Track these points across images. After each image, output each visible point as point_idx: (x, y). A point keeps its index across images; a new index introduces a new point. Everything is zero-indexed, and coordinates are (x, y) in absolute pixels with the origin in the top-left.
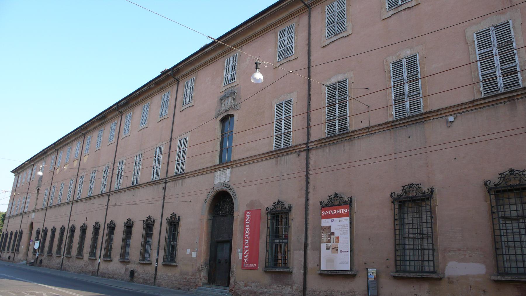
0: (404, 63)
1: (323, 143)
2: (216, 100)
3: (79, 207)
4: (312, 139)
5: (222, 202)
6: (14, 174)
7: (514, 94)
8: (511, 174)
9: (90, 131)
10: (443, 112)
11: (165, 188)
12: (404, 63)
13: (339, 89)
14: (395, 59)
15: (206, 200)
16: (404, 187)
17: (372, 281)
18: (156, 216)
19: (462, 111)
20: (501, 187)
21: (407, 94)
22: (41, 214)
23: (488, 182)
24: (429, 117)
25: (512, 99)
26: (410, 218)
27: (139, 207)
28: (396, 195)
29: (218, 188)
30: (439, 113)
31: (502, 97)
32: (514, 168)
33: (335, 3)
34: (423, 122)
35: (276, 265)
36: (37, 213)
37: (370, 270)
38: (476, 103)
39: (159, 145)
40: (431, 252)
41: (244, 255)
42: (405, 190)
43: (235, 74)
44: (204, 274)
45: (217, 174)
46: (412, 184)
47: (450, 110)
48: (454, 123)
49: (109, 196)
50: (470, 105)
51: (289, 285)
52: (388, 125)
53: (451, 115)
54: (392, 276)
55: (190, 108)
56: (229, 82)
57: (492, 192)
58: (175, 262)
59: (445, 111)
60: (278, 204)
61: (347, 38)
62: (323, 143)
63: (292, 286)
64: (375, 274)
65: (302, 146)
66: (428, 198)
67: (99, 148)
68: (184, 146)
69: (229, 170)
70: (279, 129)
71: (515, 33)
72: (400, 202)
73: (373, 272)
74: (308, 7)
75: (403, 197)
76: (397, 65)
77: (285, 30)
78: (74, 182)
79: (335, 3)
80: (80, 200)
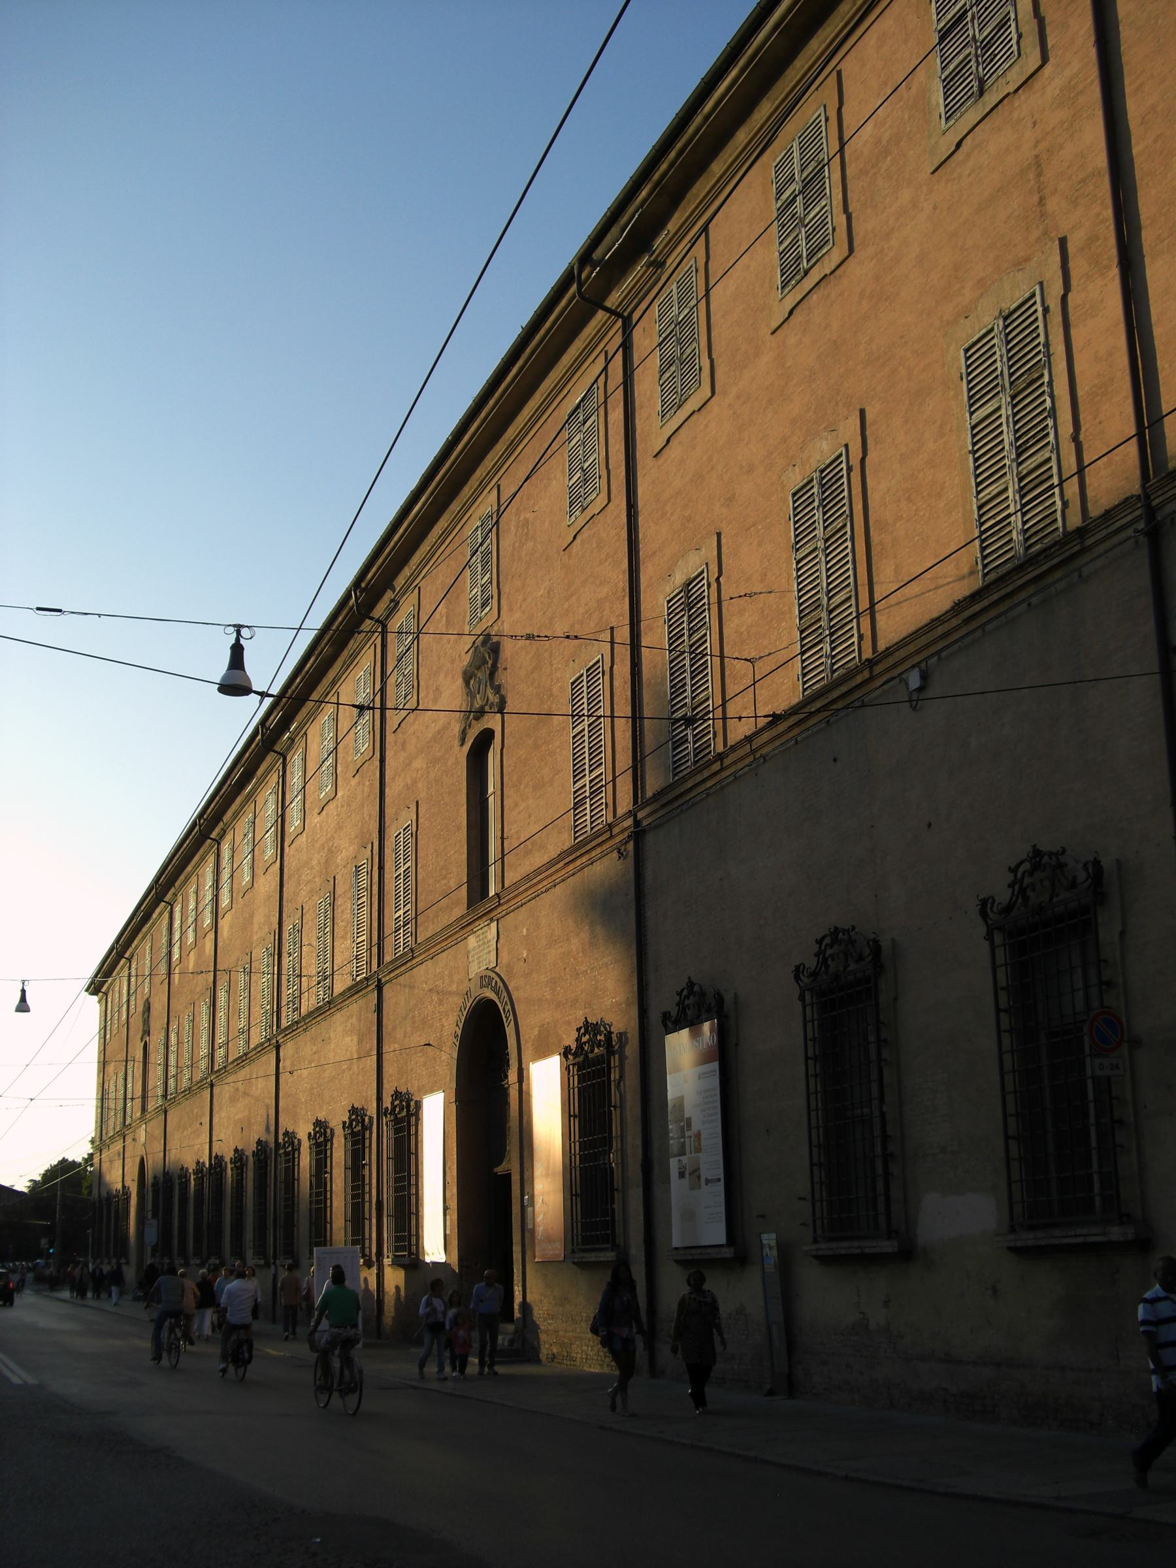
6: (95, 998)
19: (940, 645)
27: (326, 1081)
60: (1036, 867)
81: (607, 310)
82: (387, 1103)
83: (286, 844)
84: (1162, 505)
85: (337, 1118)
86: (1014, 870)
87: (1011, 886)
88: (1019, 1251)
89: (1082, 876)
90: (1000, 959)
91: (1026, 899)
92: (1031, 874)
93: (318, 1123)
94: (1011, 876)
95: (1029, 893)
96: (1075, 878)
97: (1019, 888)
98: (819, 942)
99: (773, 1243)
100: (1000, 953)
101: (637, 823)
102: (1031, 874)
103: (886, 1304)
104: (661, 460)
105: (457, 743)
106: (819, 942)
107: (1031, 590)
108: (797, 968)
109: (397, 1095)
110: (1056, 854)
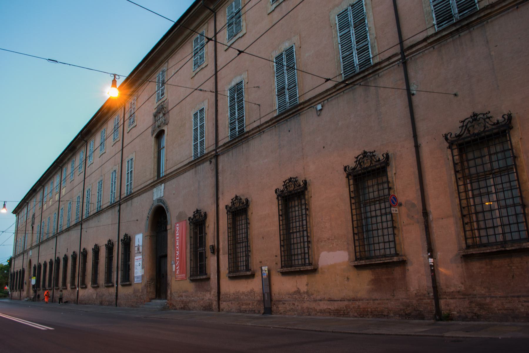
0: (284, 56)
1: (433, 42)
2: (152, 117)
3: (62, 238)
4: (220, 144)
5: (159, 216)
6: (15, 215)
7: (366, 73)
8: (473, 120)
9: (65, 163)
10: (313, 101)
11: (119, 211)
12: (284, 56)
13: (237, 91)
14: (277, 53)
15: (148, 217)
16: (357, 158)
17: (265, 279)
18: (115, 240)
19: (328, 97)
20: (357, 171)
21: (287, 87)
22: (36, 250)
23: (448, 137)
24: (303, 108)
25: (365, 79)
26: (372, 192)
27: (100, 233)
28: (453, 135)
29: (156, 204)
30: (311, 102)
31: (357, 78)
32: (367, 150)
33: (234, 3)
34: (299, 114)
35: (237, 271)
36: (33, 250)
37: (263, 268)
38: (338, 88)
39: (114, 169)
40: (390, 230)
41: (176, 267)
42: (359, 161)
43: (164, 89)
44: (152, 289)
45: (155, 190)
46: (291, 178)
47: (318, 98)
48: (323, 112)
49: (82, 225)
50: (334, 90)
51: (208, 291)
52: (273, 122)
53: (319, 103)
54: (278, 272)
55: (134, 128)
56: (160, 98)
57: (454, 147)
58: (206, 274)
59: (315, 100)
60: (364, 156)
61: (243, 37)
62: (433, 42)
63: (211, 292)
64: (267, 272)
65: (213, 153)
66: (505, 131)
67: (104, 152)
68: (131, 168)
69: (163, 185)
70: (196, 139)
71: (366, 10)
72: (355, 176)
73: (265, 268)
74: (213, 12)
75: (463, 136)
76: (279, 58)
77: (198, 38)
78: (57, 216)
79: (234, 3)
80: (62, 232)
81: (210, 9)
82: (82, 250)
83: (87, 166)
84: (408, 55)
85: (48, 261)
86: (284, 182)
87: (284, 185)
88: (356, 267)
89: (302, 183)
90: (280, 203)
91: (287, 189)
92: (363, 158)
93: (96, 245)
94: (283, 184)
95: (362, 164)
96: (379, 159)
97: (233, 203)
98: (194, 212)
99: (266, 269)
100: (280, 201)
101: (217, 153)
102: (363, 158)
103: (307, 285)
104: (227, 52)
105: (150, 135)
106: (194, 212)
107: (361, 80)
108: (276, 190)
109: (84, 249)
110: (373, 152)
